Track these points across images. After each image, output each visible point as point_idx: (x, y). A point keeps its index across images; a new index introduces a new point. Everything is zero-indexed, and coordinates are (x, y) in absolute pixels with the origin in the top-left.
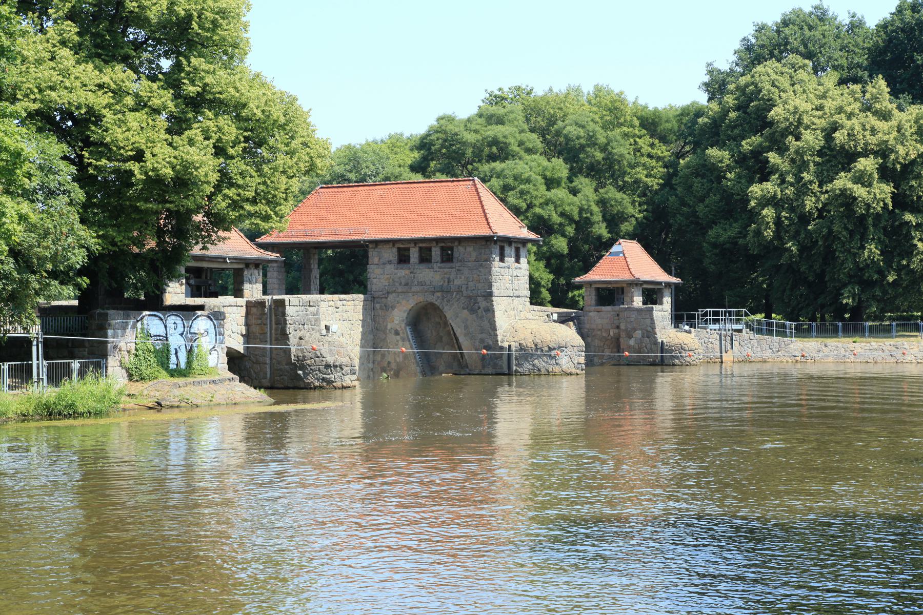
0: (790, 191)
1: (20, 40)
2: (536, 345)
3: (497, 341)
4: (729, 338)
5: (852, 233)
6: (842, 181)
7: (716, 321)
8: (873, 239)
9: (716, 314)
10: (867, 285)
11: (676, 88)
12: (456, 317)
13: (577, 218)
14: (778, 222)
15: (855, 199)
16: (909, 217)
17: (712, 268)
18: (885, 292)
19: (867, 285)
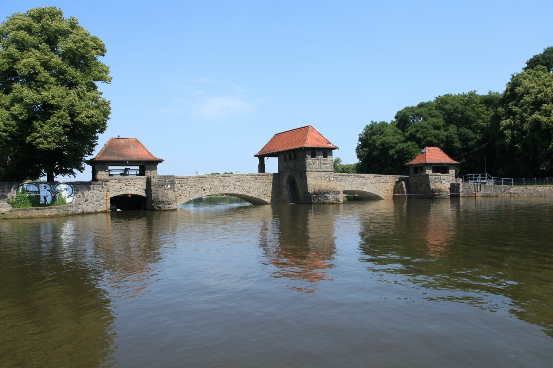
4: (479, 186)
6: (536, 115)
7: (472, 179)
9: (476, 176)
11: (500, 88)
13: (445, 140)
14: (513, 136)
15: (541, 122)
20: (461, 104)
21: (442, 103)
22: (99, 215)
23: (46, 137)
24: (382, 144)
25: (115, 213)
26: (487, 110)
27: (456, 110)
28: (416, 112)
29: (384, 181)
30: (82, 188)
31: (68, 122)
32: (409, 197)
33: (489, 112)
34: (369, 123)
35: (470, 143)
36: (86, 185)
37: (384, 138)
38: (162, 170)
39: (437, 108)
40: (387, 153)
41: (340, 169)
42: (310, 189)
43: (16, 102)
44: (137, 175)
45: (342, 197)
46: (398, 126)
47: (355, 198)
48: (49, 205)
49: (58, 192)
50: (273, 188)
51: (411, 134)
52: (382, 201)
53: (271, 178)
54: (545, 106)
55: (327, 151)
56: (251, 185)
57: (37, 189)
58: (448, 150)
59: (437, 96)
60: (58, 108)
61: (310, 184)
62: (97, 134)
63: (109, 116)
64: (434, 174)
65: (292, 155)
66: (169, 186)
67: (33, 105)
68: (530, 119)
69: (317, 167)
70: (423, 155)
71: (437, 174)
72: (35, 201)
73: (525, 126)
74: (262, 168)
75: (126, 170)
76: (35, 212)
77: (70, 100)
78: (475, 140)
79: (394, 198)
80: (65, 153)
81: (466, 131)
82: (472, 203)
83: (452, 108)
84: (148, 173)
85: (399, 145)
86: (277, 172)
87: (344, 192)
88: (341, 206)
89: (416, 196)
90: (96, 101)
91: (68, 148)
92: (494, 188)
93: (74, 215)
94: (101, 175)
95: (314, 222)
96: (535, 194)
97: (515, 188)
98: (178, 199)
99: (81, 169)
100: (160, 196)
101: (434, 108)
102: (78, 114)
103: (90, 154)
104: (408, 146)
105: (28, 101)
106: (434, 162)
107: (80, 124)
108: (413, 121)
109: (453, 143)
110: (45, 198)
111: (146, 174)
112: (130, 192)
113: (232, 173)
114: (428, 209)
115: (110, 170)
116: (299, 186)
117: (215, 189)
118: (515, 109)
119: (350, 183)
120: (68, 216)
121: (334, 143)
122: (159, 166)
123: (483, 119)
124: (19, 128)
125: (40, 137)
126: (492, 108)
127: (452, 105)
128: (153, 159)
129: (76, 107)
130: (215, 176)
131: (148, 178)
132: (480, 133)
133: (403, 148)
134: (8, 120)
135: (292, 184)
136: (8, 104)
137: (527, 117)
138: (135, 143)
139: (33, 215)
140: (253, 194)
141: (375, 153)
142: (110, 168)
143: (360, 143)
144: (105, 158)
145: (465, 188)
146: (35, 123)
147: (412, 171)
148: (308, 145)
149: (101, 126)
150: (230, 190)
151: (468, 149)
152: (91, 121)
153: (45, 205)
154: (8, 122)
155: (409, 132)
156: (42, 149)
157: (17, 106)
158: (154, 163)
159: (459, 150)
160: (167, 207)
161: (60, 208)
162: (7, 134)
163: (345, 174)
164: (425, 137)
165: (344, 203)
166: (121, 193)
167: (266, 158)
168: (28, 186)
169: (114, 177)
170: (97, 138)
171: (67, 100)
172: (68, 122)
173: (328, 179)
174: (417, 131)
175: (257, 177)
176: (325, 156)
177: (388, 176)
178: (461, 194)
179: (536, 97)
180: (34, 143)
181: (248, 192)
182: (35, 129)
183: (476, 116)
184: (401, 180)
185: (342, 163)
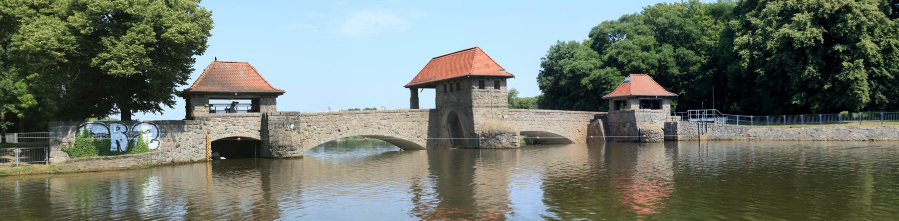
0: (759, 39)
5: (797, 61)
6: (786, 29)
7: (694, 117)
8: (812, 63)
9: (701, 112)
10: (811, 92)
12: (462, 118)
13: (657, 65)
14: (752, 58)
16: (839, 48)
17: (731, 87)
18: (825, 96)
19: (811, 92)
20: (679, 16)
21: (651, 16)
22: (195, 165)
23: (120, 59)
24: (572, 71)
25: (217, 162)
26: (715, 23)
27: (672, 25)
28: (618, 27)
30: (171, 129)
31: (152, 38)
32: (609, 140)
33: (718, 27)
34: (555, 44)
35: (691, 68)
36: (177, 125)
37: (575, 63)
38: (282, 105)
39: (645, 22)
40: (579, 82)
41: (516, 104)
42: (478, 129)
43: (76, 10)
44: (249, 111)
45: (519, 140)
46: (592, 47)
47: (537, 142)
48: (124, 153)
49: (138, 134)
50: (430, 128)
51: (611, 58)
52: (572, 145)
53: (427, 115)
54: (798, 17)
55: (499, 81)
57: (107, 132)
58: (662, 78)
59: (646, 6)
60: (138, 19)
62: (194, 56)
63: (211, 32)
65: (454, 85)
66: (292, 126)
67: (100, 14)
68: (776, 35)
71: (646, 110)
72: (104, 148)
73: (770, 45)
74: (415, 102)
75: (234, 104)
76: (104, 163)
77: (155, 10)
78: (699, 65)
79: (588, 141)
80: (148, 81)
81: (686, 52)
82: (694, 148)
83: (666, 21)
84: (264, 109)
85: (595, 72)
86: (434, 107)
87: (522, 134)
88: (518, 152)
89: (618, 140)
90: (192, 12)
91: (152, 74)
92: (726, 129)
93: (160, 166)
94: (199, 111)
95: (483, 177)
96: (785, 138)
97: (755, 130)
98: (303, 143)
99: (170, 104)
100: (280, 139)
101: (641, 22)
102: (167, 28)
103: (183, 83)
104: (607, 73)
105: (93, 9)
107: (170, 42)
108: (614, 40)
109: (668, 68)
110: (118, 142)
111: (262, 110)
112: (239, 134)
113: (375, 109)
114: (634, 157)
115: (212, 105)
116: (463, 126)
117: (354, 129)
118: (754, 21)
120: (151, 167)
121: (509, 70)
122: (279, 99)
123: (709, 35)
124: (81, 46)
125: (111, 59)
126: (723, 21)
127: (667, 18)
128: (270, 90)
129: (164, 19)
130: (354, 112)
131: (263, 115)
132: (705, 55)
133: (600, 77)
134: (64, 34)
135: (454, 123)
136: (63, 11)
137: (771, 32)
138: (246, 68)
139: (101, 167)
140: (403, 136)
141: (563, 83)
142: (211, 102)
143: (543, 69)
144: (204, 89)
145: (686, 128)
146: (103, 39)
147: (611, 105)
148: (475, 72)
149: (199, 46)
150: (373, 131)
151: (689, 77)
152: (185, 38)
153: (118, 153)
154: (64, 38)
155: (608, 55)
156: (114, 75)
157: (77, 15)
158: (272, 96)
159: (676, 78)
160: (289, 154)
161: (140, 157)
162: (63, 54)
163: (523, 110)
164: (630, 61)
165: (521, 147)
166: (227, 135)
167: (420, 90)
168: (93, 126)
169: (217, 114)
170: (194, 61)
171: (151, 8)
172: (152, 38)
173: (500, 117)
174: (619, 53)
176: (497, 87)
178: (679, 137)
179: (786, 5)
180: (102, 67)
181: (397, 133)
182: (103, 47)
183: (700, 32)
184: (596, 117)
185: (519, 96)
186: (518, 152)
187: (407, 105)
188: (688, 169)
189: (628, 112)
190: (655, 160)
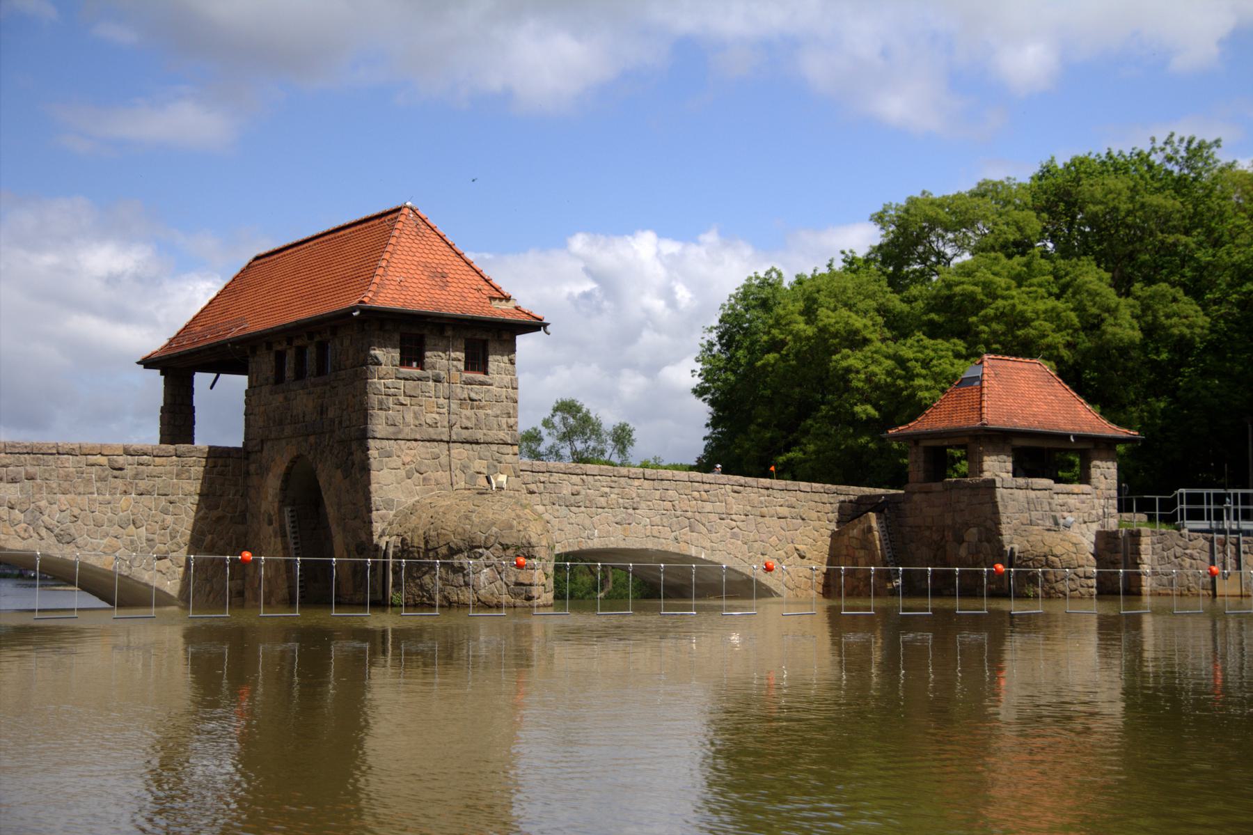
1: (978, 274)
2: (427, 542)
3: (371, 534)
4: (1230, 549)
7: (1196, 515)
9: (1220, 499)
12: (329, 479)
29: (784, 511)
42: (385, 528)
52: (769, 611)
56: (83, 501)
61: (389, 504)
64: (1021, 481)
69: (430, 418)
70: (970, 394)
95: (402, 721)
106: (1020, 423)
119: (621, 514)
145: (1163, 554)
167: (202, 380)
175: (121, 460)
177: (804, 485)
181: (64, 538)
186: (546, 622)
187: (149, 434)
188: (1173, 692)
189: (975, 487)
190: (1066, 668)
